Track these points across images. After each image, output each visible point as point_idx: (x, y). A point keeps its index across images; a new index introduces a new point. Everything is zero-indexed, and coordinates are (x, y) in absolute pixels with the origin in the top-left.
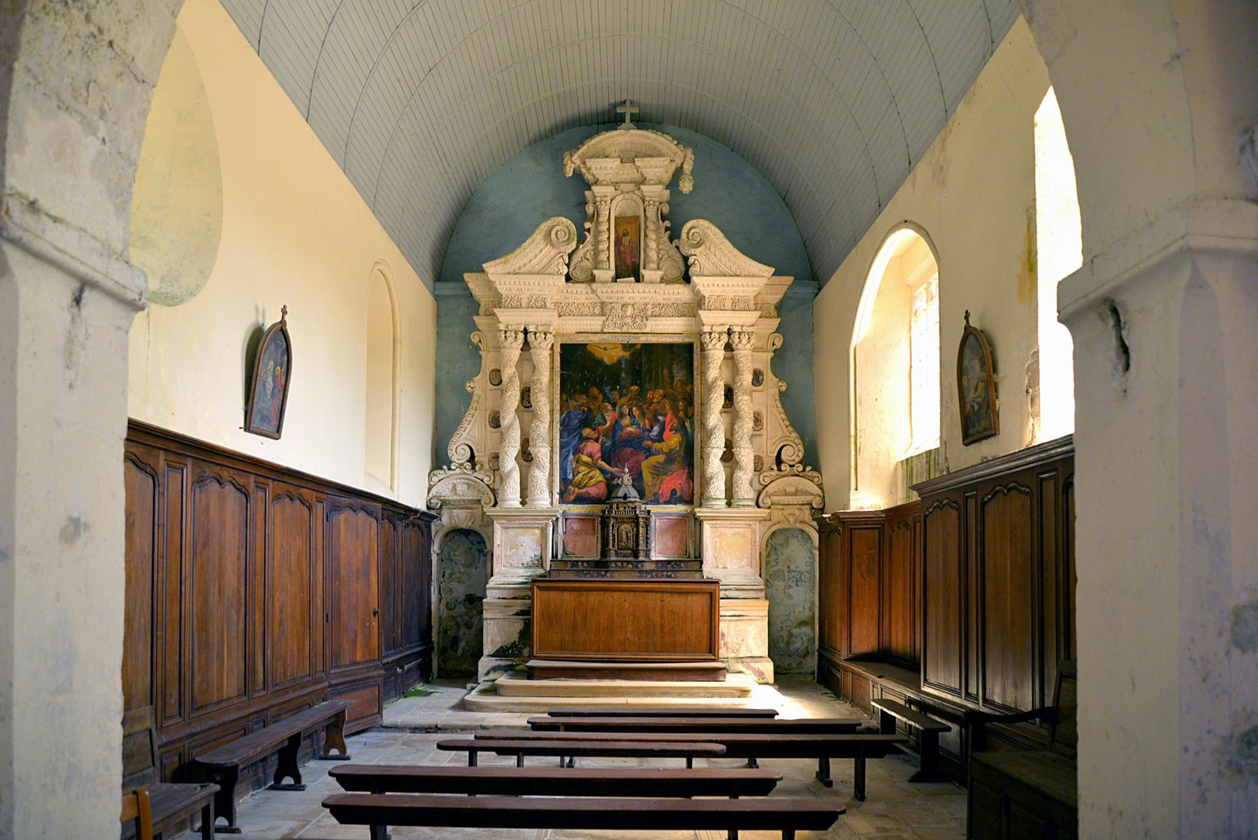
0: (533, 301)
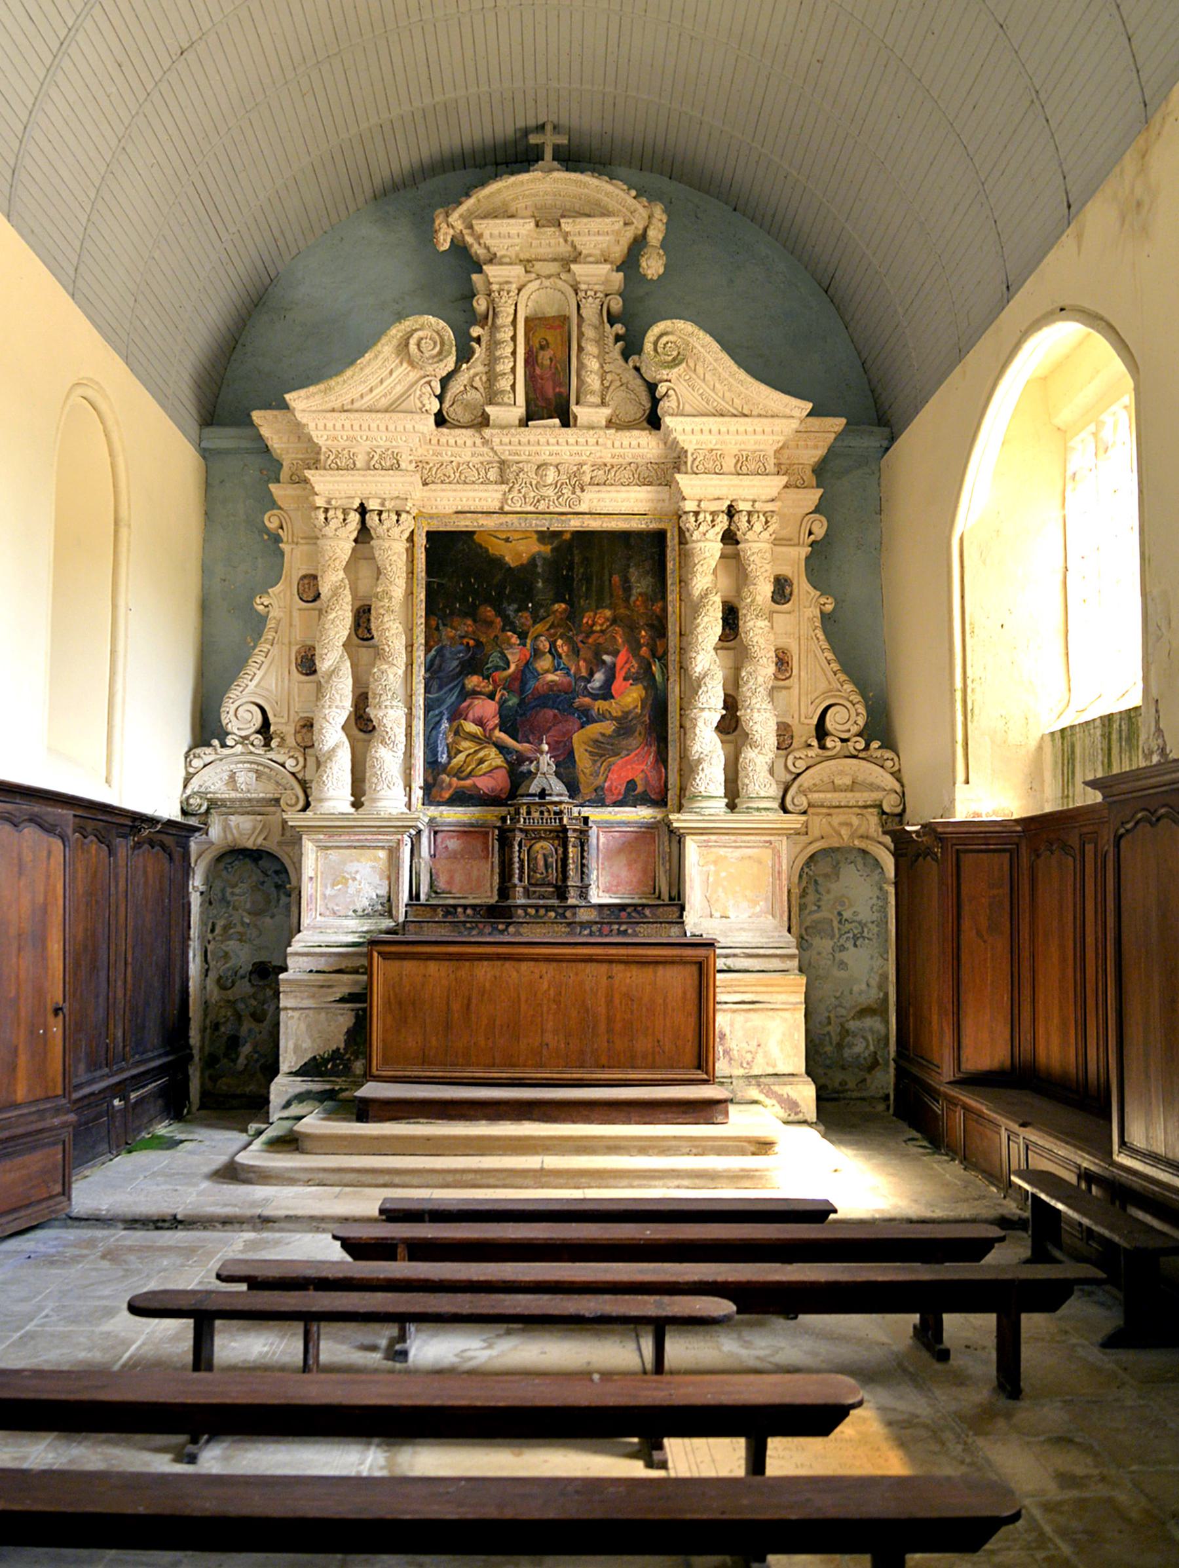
0: (376, 458)
